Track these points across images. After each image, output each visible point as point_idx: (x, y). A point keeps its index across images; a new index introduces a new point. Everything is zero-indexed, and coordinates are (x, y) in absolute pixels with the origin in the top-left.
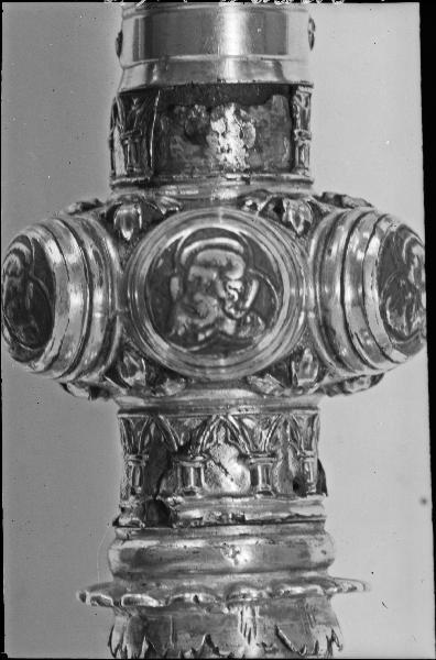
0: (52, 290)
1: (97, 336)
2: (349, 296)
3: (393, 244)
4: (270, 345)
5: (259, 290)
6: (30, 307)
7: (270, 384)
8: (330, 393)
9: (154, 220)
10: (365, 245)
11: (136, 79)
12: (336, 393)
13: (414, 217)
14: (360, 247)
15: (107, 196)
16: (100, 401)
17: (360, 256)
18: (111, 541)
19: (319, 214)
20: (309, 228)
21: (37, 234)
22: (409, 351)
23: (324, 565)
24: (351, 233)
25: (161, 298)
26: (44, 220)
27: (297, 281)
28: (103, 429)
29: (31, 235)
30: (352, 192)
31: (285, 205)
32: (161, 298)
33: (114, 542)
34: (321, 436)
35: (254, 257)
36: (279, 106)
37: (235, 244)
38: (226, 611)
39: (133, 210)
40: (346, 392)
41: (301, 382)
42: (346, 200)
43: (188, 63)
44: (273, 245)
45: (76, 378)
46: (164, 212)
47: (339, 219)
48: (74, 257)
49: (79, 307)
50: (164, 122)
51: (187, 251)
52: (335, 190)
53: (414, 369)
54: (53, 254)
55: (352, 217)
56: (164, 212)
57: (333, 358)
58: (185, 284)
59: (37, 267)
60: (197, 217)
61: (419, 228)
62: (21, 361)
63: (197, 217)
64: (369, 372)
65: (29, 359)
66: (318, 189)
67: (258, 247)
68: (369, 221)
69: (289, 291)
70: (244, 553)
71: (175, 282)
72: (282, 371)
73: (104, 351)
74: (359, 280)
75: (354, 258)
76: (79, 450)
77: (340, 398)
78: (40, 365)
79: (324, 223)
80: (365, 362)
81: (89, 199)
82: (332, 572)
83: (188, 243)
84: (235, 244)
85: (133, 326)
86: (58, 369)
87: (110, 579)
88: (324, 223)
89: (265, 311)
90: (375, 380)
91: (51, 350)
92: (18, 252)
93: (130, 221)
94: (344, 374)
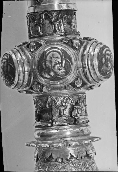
2: (89, 63)
4: (71, 78)
5: (66, 62)
6: (10, 73)
8: (88, 90)
9: (39, 45)
11: (32, 10)
12: (89, 89)
13: (108, 41)
14: (92, 51)
16: (28, 95)
17: (92, 53)
18: (34, 131)
19: (82, 43)
20: (80, 47)
22: (106, 75)
23: (88, 134)
25: (41, 66)
26: (11, 49)
27: (76, 61)
28: (29, 104)
30: (90, 36)
32: (41, 66)
33: (35, 131)
35: (65, 55)
37: (59, 51)
38: (66, 41)
40: (93, 89)
41: (78, 86)
44: (70, 52)
49: (22, 71)
50: (41, 21)
52: (86, 36)
53: (110, 83)
54: (14, 57)
58: (105, 59)
59: (10, 60)
60: (48, 45)
62: (8, 86)
63: (48, 45)
65: (9, 85)
66: (82, 37)
67: (67, 52)
69: (74, 64)
71: (104, 59)
74: (92, 60)
75: (91, 55)
76: (19, 108)
77: (91, 90)
78: (12, 87)
79: (85, 44)
81: (24, 42)
82: (91, 135)
83: (48, 50)
87: (35, 140)
88: (85, 44)
90: (99, 85)
93: (33, 47)
94: (91, 85)
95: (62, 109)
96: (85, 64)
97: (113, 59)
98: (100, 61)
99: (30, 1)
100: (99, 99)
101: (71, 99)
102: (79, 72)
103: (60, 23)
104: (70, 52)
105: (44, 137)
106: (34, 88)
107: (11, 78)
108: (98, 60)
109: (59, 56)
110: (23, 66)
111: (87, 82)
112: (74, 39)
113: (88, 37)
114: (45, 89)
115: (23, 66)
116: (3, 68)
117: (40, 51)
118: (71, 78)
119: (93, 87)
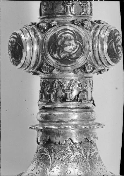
0: (23, 45)
1: (34, 59)
3: (112, 37)
4: (81, 61)
6: (17, 50)
7: (80, 72)
9: (50, 26)
10: (104, 33)
14: (103, 34)
15: (38, 21)
21: (19, 32)
24: (101, 30)
29: (17, 32)
30: (103, 20)
31: (84, 23)
32: (54, 45)
34: (40, 85)
35: (77, 37)
36: (72, 91)
39: (44, 25)
40: (101, 73)
42: (101, 22)
43: (69, 60)
44: (82, 32)
45: (29, 70)
46: (52, 25)
47: (98, 27)
48: (27, 39)
49: (31, 51)
51: (59, 36)
54: (23, 37)
55: (102, 25)
56: (52, 25)
57: (97, 65)
61: (119, 29)
64: (107, 68)
68: (105, 27)
70: (75, 116)
72: (83, 68)
73: (37, 62)
74: (102, 45)
78: (20, 66)
80: (106, 66)
84: (72, 33)
85: (44, 55)
86: (24, 67)
89: (81, 50)
91: (22, 61)
92: (14, 37)
95: (69, 6)
96: (95, 47)
97: (121, 34)
98: (109, 44)
99: (40, 2)
100: (107, 87)
101: (79, 44)
102: (90, 57)
103: (73, 4)
104: (82, 32)
105: (46, 119)
106: (44, 71)
107: (19, 58)
108: (107, 44)
109: (72, 37)
110: (32, 44)
111: (96, 65)
112: (86, 20)
113: (101, 21)
114: (55, 71)
115: (32, 44)
116: (9, 48)
117: (50, 33)
118: (81, 61)
119: (102, 72)
